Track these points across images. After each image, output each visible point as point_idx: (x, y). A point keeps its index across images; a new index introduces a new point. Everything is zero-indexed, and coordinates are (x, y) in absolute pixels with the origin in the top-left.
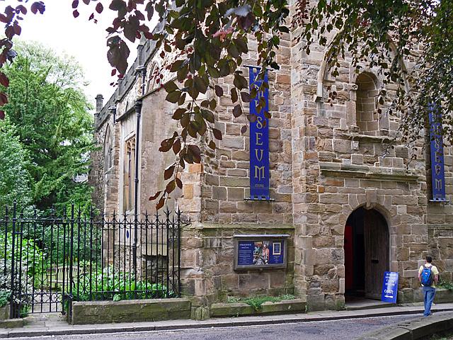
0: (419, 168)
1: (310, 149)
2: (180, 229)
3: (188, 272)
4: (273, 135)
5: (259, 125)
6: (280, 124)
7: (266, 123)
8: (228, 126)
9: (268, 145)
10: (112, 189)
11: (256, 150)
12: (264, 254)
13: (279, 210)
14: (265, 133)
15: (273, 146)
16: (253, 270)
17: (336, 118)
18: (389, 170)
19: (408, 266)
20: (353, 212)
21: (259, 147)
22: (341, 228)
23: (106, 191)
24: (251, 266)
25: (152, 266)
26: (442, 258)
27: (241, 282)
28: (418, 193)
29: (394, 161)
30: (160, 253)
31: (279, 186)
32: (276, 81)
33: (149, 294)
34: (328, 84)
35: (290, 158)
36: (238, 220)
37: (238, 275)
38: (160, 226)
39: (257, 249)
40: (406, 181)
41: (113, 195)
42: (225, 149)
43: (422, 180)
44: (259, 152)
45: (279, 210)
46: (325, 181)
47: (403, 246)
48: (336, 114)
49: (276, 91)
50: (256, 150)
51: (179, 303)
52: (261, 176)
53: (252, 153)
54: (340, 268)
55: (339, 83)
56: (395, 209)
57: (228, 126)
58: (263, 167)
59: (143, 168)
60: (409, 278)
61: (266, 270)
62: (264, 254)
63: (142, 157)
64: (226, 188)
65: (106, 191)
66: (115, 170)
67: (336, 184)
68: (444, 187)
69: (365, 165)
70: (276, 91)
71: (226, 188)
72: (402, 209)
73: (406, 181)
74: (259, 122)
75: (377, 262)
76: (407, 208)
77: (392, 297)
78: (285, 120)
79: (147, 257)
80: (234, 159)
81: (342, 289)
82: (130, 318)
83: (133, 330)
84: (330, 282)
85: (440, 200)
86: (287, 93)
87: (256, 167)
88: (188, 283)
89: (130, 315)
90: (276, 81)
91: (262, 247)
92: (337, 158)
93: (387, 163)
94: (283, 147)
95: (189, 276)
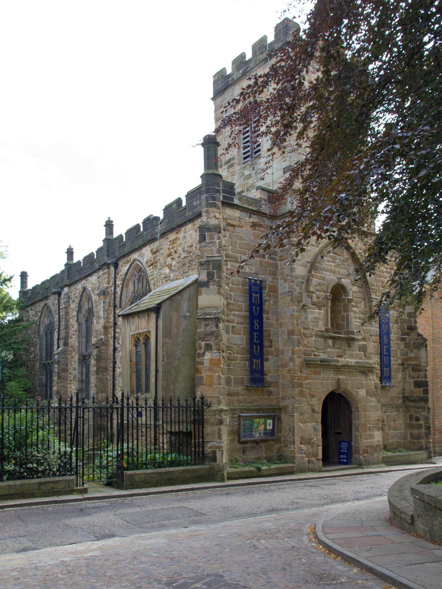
0: (374, 360)
1: (297, 346)
2: (203, 410)
3: (210, 445)
4: (265, 334)
5: (257, 327)
6: (271, 325)
7: (261, 324)
8: (233, 327)
9: (263, 343)
10: (62, 368)
11: (255, 347)
12: (260, 429)
13: (270, 393)
14: (261, 331)
15: (266, 343)
16: (252, 442)
17: (316, 321)
18: (352, 361)
19: (367, 436)
20: (328, 395)
21: (256, 344)
22: (319, 408)
23: (56, 370)
24: (252, 439)
25: (175, 440)
26: (388, 430)
27: (244, 451)
28: (374, 379)
29: (357, 354)
30: (181, 429)
31: (270, 375)
32: (267, 290)
33: (172, 464)
34: (310, 294)
35: (278, 352)
36: (240, 402)
37: (242, 446)
38: (148, 409)
39: (255, 425)
40: (365, 370)
41: (64, 374)
42: (231, 345)
43: (377, 370)
44: (256, 348)
45: (270, 393)
46: (308, 371)
47: (363, 421)
48: (316, 318)
49: (267, 298)
50: (255, 347)
51: (203, 469)
52: (258, 367)
53: (251, 348)
54: (318, 438)
55: (318, 293)
56: (357, 393)
57: (233, 327)
58: (259, 360)
59: (163, 360)
60: (368, 446)
61: (262, 441)
62: (260, 429)
63: (163, 351)
64: (232, 377)
65: (56, 370)
66: (66, 351)
67: (316, 373)
68: (390, 374)
69: (336, 358)
70: (267, 298)
71: (232, 377)
72: (362, 393)
73: (365, 370)
74: (256, 324)
75: (340, 433)
76: (367, 392)
77: (345, 461)
78: (274, 322)
79: (171, 433)
80: (237, 353)
81: (320, 456)
82: (170, 482)
83: (178, 491)
84: (311, 450)
85: (387, 384)
86: (276, 300)
87: (255, 360)
88: (211, 453)
89: (169, 480)
90: (267, 290)
91: (259, 424)
92: (316, 353)
93: (352, 356)
94: (273, 343)
95: (211, 447)
